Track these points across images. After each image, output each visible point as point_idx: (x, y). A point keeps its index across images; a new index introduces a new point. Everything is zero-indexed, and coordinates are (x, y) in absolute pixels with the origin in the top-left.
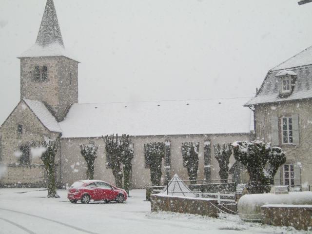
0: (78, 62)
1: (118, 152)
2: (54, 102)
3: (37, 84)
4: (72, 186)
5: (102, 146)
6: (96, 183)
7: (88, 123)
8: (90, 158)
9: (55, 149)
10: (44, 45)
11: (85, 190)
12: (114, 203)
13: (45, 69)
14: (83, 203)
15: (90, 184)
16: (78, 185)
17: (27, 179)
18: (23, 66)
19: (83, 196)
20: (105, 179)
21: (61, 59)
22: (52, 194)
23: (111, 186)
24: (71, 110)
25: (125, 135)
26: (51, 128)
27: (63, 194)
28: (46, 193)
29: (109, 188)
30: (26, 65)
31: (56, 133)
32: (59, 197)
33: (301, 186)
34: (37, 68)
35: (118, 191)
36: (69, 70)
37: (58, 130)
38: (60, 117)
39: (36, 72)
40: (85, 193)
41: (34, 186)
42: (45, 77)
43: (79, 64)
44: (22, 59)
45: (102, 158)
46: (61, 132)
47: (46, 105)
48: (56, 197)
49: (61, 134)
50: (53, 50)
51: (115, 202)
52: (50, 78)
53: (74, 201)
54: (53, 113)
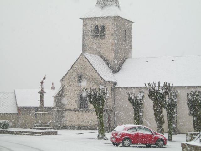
0: (132, 22)
1: (162, 97)
2: (111, 56)
3: (97, 41)
4: (114, 130)
5: (147, 92)
6: (137, 128)
7: (136, 76)
8: (137, 105)
9: (104, 96)
10: (102, 8)
11: (126, 134)
12: (144, 147)
13: (103, 28)
14: (124, 146)
15: (131, 129)
16: (120, 129)
17: (86, 122)
18: (85, 25)
19: (123, 140)
20: (150, 125)
21: (117, 18)
22: (101, 137)
23: (151, 132)
24: (125, 65)
25: (167, 83)
26: (106, 79)
27: (108, 135)
28: (94, 134)
29: (150, 133)
30: (88, 25)
31: (112, 83)
32: (107, 139)
33: (171, 135)
34: (97, 27)
35: (158, 136)
36: (124, 29)
37: (112, 80)
38: (116, 69)
39: (96, 31)
40: (126, 137)
41: (91, 128)
42: (103, 35)
43: (133, 24)
44: (83, 19)
45: (149, 104)
46: (116, 82)
47: (103, 58)
48: (104, 139)
49: (115, 84)
50: (111, 11)
51: (145, 146)
52: (109, 35)
53: (116, 143)
54: (110, 67)
